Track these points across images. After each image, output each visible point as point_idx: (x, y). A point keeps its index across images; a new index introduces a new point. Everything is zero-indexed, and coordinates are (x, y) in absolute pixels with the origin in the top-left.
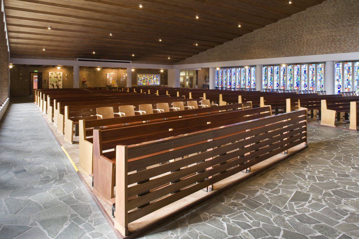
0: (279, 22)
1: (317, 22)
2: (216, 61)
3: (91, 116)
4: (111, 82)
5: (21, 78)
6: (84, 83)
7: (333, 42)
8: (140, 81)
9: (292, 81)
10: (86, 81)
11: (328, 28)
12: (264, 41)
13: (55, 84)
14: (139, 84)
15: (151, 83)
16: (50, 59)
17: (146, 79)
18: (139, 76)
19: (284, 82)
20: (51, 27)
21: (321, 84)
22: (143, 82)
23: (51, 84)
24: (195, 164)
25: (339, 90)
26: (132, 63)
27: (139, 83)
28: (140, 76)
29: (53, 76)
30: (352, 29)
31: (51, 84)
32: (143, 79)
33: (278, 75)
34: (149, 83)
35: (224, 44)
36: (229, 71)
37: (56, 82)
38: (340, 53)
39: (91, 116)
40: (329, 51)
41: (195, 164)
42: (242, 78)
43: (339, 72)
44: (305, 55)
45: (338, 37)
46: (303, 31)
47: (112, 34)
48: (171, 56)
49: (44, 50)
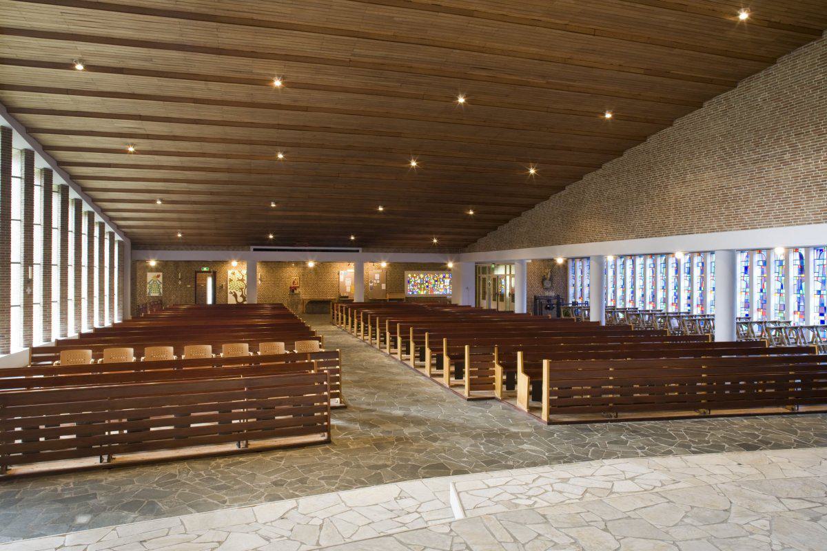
0: (625, 155)
1: (692, 153)
2: (524, 247)
3: (741, 383)
4: (348, 289)
5: (180, 283)
6: (293, 291)
7: (724, 202)
8: (413, 286)
9: (784, 295)
10: (298, 287)
11: (714, 169)
12: (600, 201)
13: (239, 294)
14: (410, 293)
15: (438, 290)
16: (202, 249)
17: (426, 282)
18: (410, 275)
19: (701, 295)
20: (161, 200)
21: (782, 303)
22: (420, 289)
23: (232, 293)
24: (42, 376)
25: (822, 318)
26: (363, 251)
27: (410, 291)
28: (412, 276)
29: (235, 278)
30: (760, 169)
31: (232, 293)
32: (419, 281)
33: (747, 278)
34: (432, 289)
35: (537, 207)
36: (798, 257)
37: (242, 289)
38: (737, 230)
39: (741, 383)
40: (715, 225)
41: (42, 376)
42: (775, 285)
43: (821, 271)
44: (672, 234)
45: (734, 191)
46: (668, 177)
47: (276, 203)
48: (438, 236)
49: (180, 235)
